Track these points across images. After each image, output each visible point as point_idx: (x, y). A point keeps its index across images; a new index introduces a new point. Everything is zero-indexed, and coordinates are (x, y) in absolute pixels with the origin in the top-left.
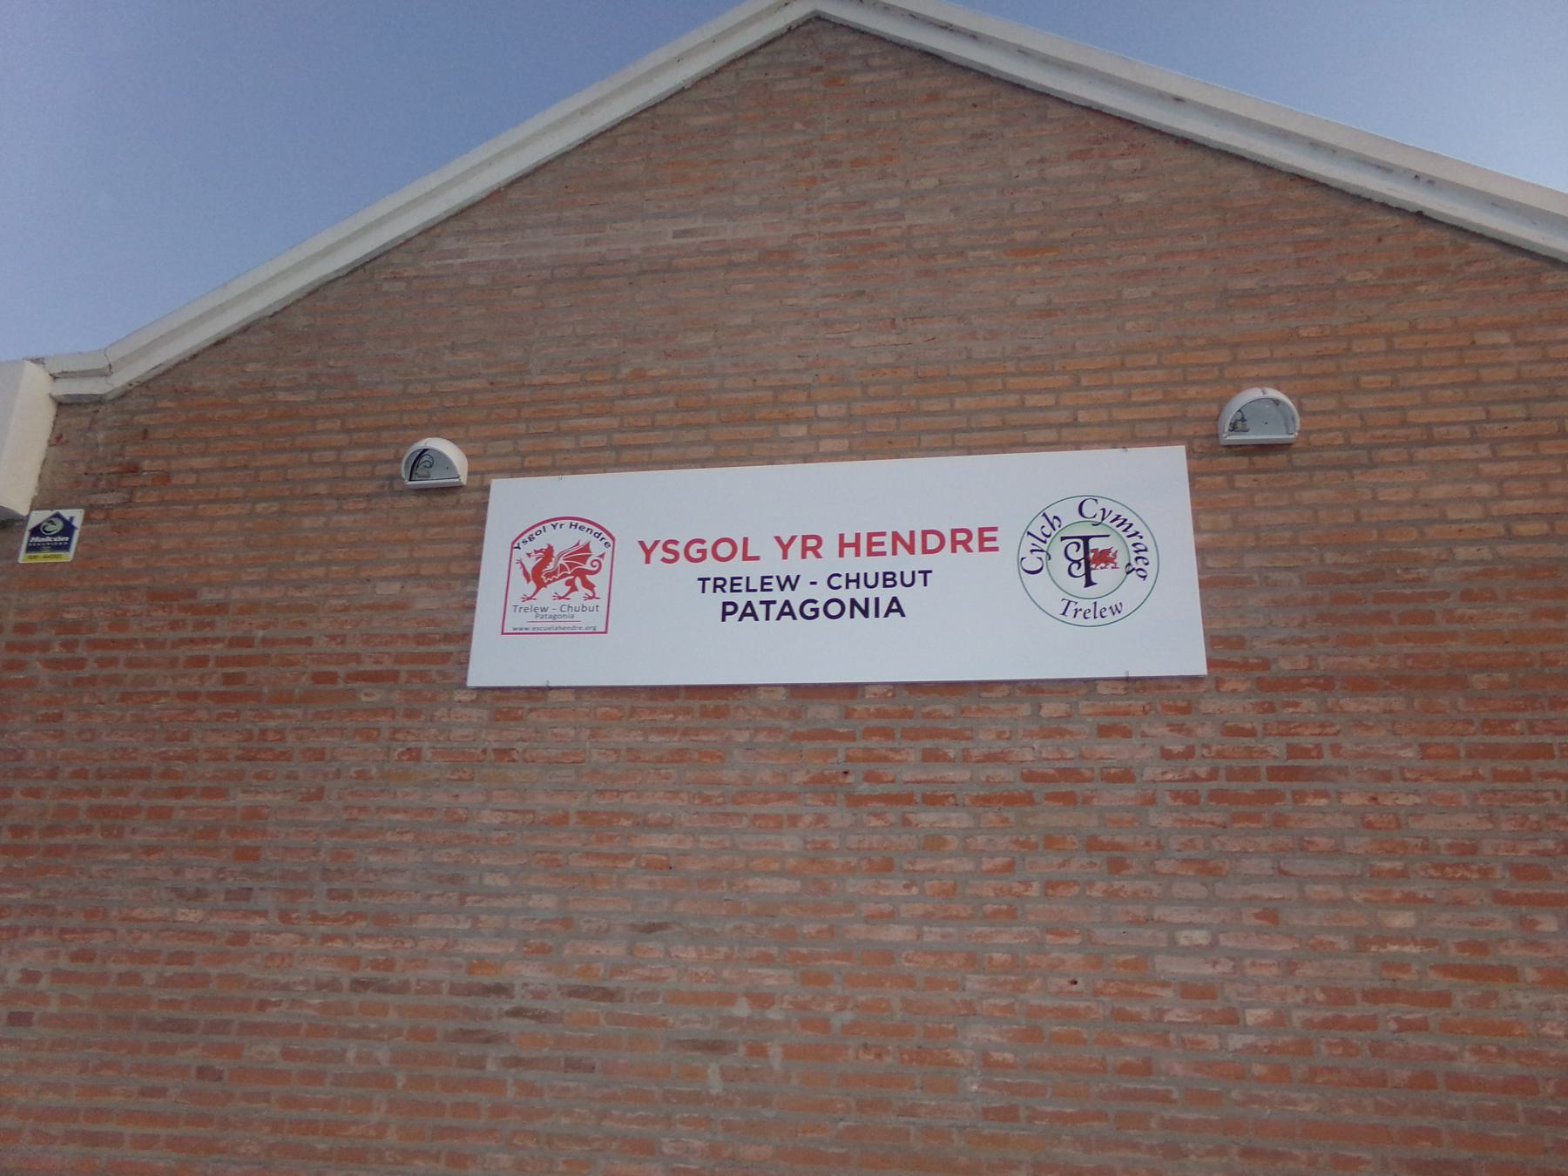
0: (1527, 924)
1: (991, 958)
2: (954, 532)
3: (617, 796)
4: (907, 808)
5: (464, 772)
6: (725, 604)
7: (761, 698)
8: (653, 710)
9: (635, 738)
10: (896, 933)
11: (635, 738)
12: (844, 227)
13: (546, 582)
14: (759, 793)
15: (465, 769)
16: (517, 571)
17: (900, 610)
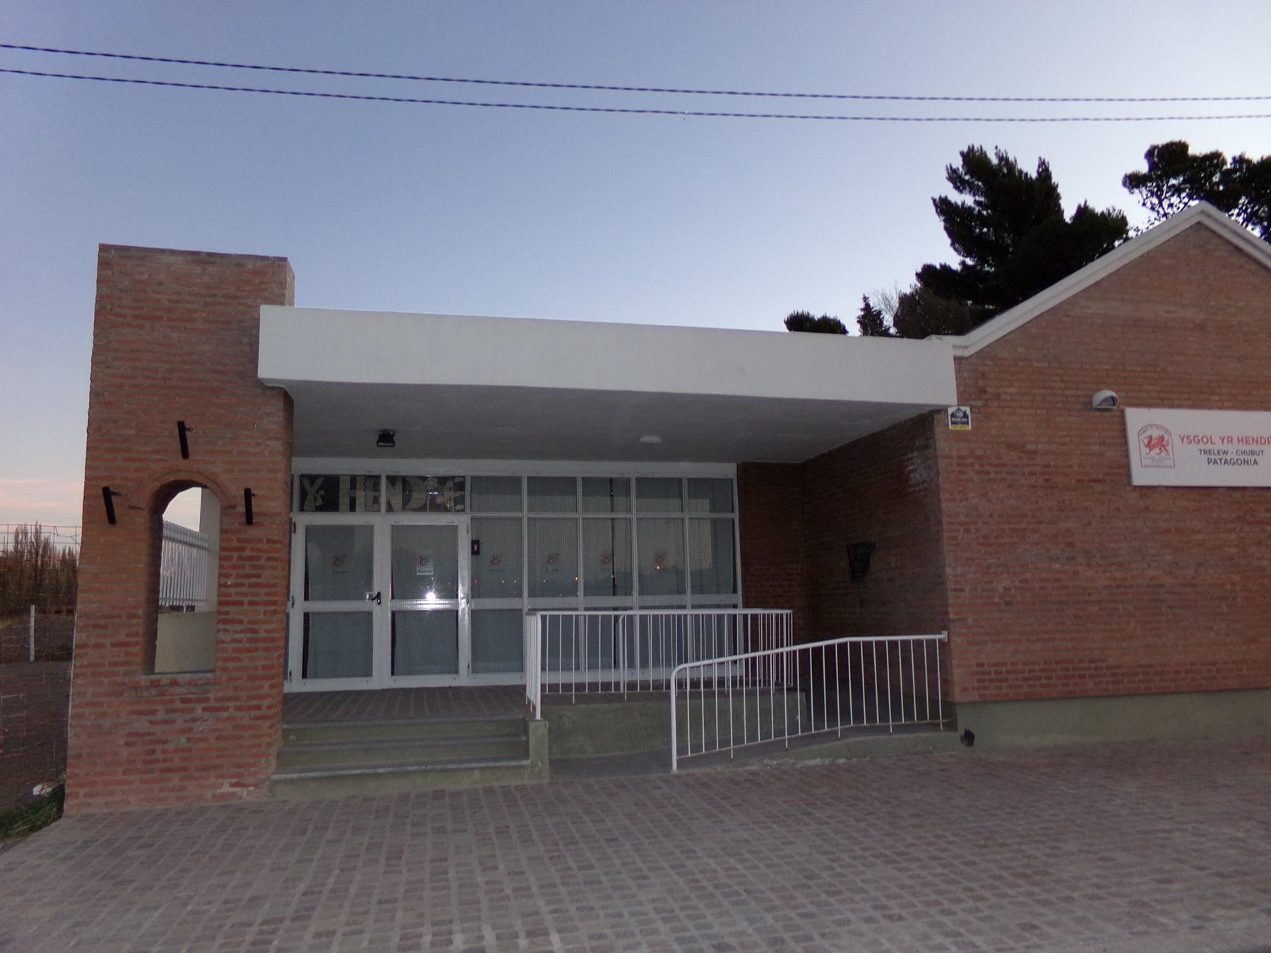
6: (1208, 460)
12: (1218, 318)
16: (1142, 444)
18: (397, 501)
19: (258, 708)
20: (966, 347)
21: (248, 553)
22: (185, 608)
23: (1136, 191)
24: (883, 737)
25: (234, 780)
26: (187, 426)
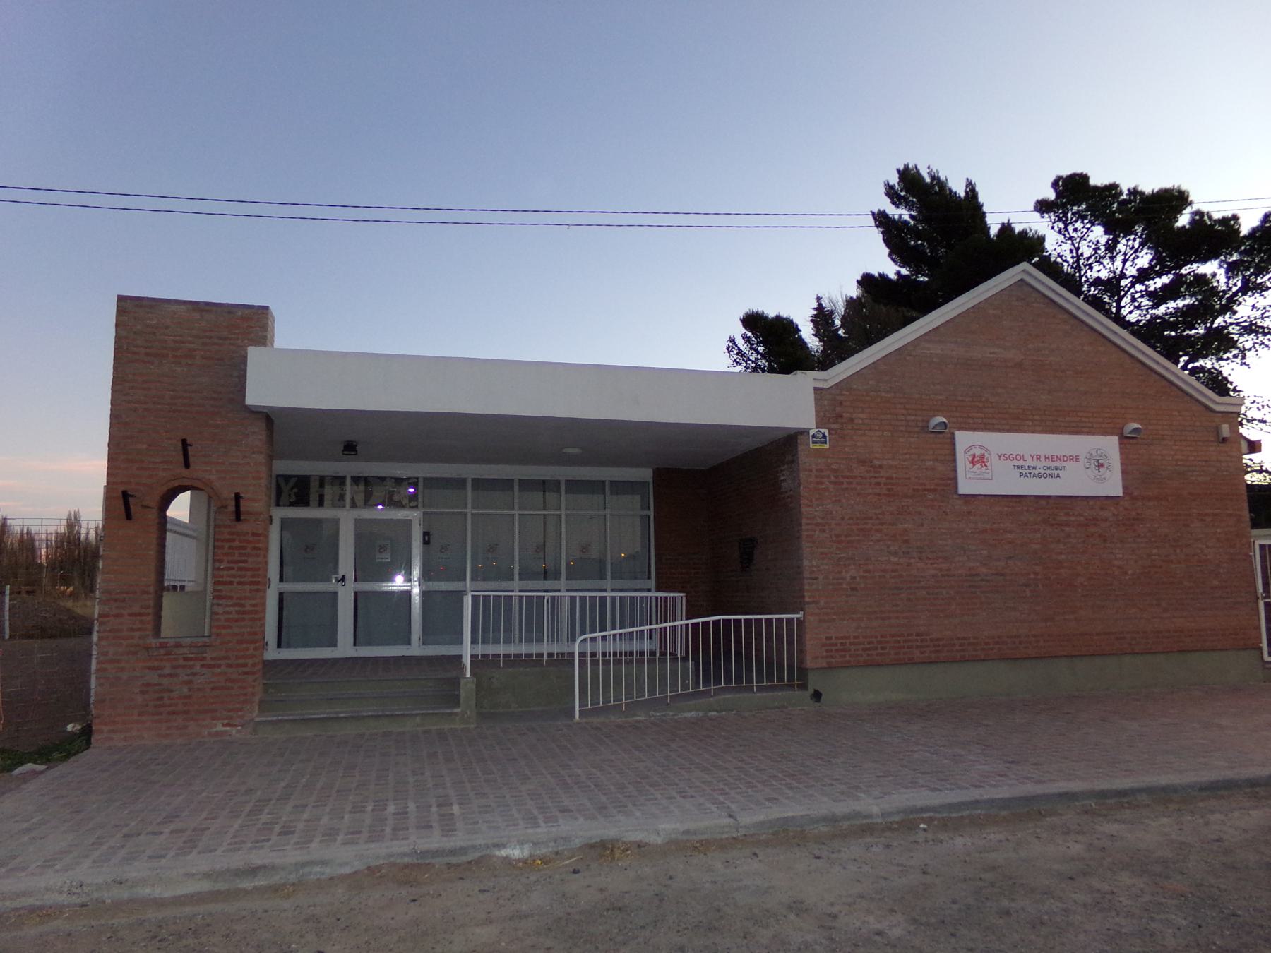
0: (1175, 551)
2: (1070, 456)
16: (967, 461)
18: (360, 498)
19: (245, 665)
20: (826, 380)
21: (237, 543)
22: (179, 588)
23: (1046, 215)
24: (750, 695)
25: (226, 721)
26: (188, 442)
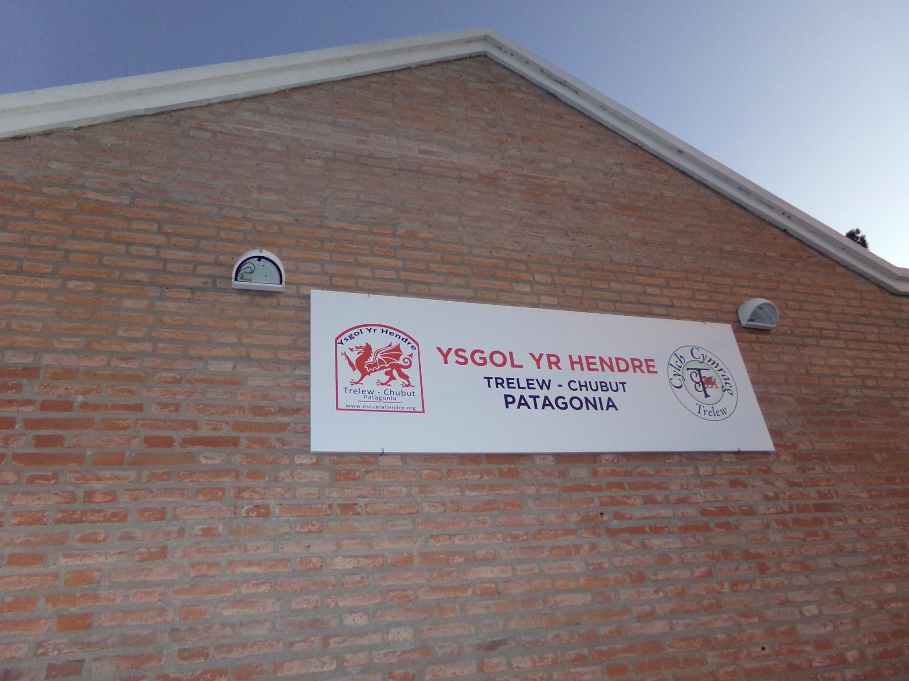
1: (716, 638)
3: (450, 539)
4: (643, 536)
5: (313, 525)
7: (538, 463)
8: (464, 472)
9: (454, 493)
10: (658, 627)
11: (454, 493)
12: (525, 172)
13: (369, 371)
14: (551, 530)
15: (314, 522)
16: (343, 362)
17: (614, 406)
